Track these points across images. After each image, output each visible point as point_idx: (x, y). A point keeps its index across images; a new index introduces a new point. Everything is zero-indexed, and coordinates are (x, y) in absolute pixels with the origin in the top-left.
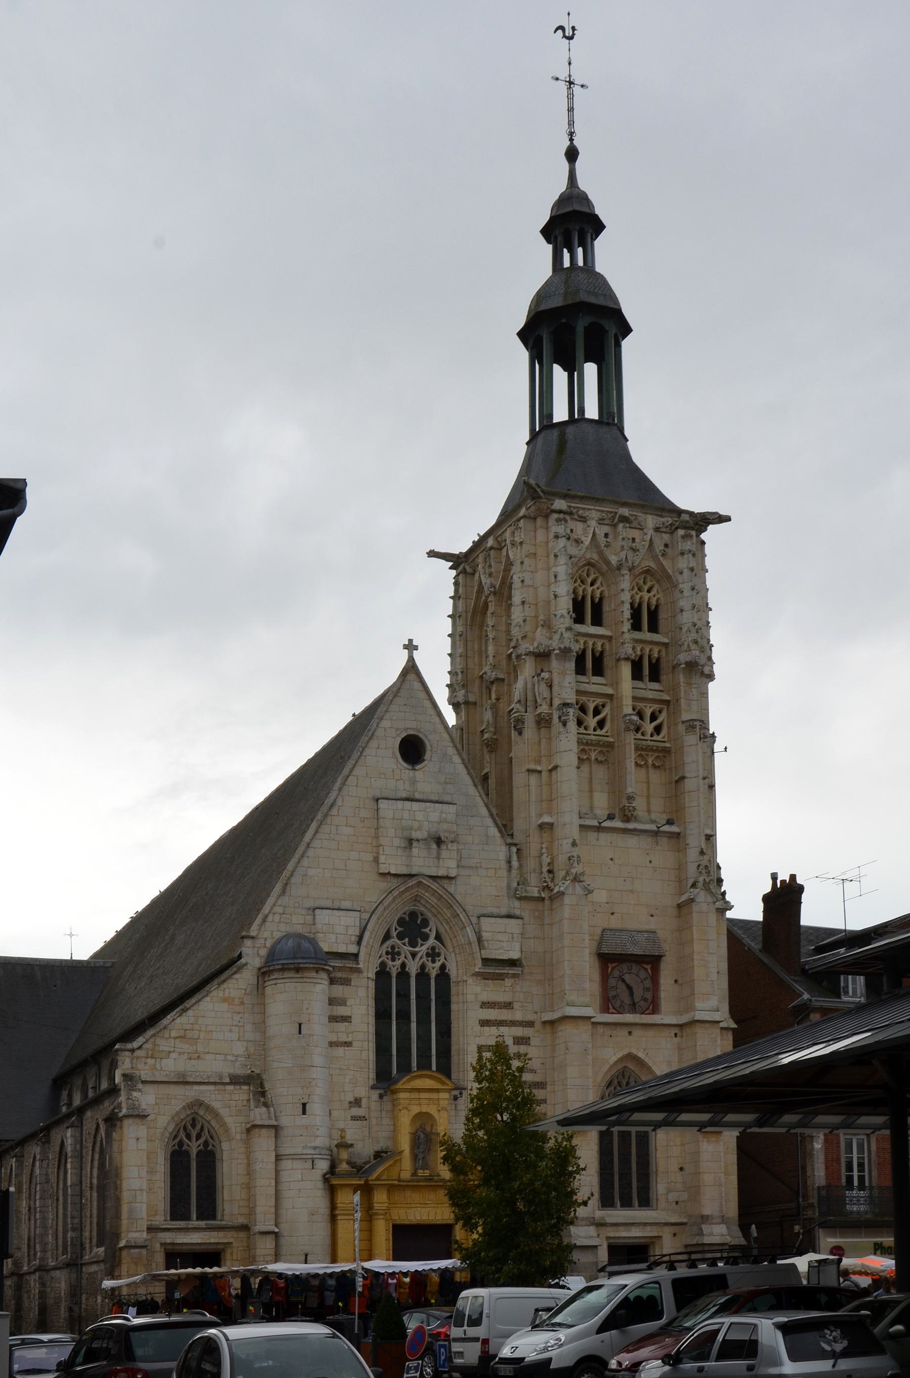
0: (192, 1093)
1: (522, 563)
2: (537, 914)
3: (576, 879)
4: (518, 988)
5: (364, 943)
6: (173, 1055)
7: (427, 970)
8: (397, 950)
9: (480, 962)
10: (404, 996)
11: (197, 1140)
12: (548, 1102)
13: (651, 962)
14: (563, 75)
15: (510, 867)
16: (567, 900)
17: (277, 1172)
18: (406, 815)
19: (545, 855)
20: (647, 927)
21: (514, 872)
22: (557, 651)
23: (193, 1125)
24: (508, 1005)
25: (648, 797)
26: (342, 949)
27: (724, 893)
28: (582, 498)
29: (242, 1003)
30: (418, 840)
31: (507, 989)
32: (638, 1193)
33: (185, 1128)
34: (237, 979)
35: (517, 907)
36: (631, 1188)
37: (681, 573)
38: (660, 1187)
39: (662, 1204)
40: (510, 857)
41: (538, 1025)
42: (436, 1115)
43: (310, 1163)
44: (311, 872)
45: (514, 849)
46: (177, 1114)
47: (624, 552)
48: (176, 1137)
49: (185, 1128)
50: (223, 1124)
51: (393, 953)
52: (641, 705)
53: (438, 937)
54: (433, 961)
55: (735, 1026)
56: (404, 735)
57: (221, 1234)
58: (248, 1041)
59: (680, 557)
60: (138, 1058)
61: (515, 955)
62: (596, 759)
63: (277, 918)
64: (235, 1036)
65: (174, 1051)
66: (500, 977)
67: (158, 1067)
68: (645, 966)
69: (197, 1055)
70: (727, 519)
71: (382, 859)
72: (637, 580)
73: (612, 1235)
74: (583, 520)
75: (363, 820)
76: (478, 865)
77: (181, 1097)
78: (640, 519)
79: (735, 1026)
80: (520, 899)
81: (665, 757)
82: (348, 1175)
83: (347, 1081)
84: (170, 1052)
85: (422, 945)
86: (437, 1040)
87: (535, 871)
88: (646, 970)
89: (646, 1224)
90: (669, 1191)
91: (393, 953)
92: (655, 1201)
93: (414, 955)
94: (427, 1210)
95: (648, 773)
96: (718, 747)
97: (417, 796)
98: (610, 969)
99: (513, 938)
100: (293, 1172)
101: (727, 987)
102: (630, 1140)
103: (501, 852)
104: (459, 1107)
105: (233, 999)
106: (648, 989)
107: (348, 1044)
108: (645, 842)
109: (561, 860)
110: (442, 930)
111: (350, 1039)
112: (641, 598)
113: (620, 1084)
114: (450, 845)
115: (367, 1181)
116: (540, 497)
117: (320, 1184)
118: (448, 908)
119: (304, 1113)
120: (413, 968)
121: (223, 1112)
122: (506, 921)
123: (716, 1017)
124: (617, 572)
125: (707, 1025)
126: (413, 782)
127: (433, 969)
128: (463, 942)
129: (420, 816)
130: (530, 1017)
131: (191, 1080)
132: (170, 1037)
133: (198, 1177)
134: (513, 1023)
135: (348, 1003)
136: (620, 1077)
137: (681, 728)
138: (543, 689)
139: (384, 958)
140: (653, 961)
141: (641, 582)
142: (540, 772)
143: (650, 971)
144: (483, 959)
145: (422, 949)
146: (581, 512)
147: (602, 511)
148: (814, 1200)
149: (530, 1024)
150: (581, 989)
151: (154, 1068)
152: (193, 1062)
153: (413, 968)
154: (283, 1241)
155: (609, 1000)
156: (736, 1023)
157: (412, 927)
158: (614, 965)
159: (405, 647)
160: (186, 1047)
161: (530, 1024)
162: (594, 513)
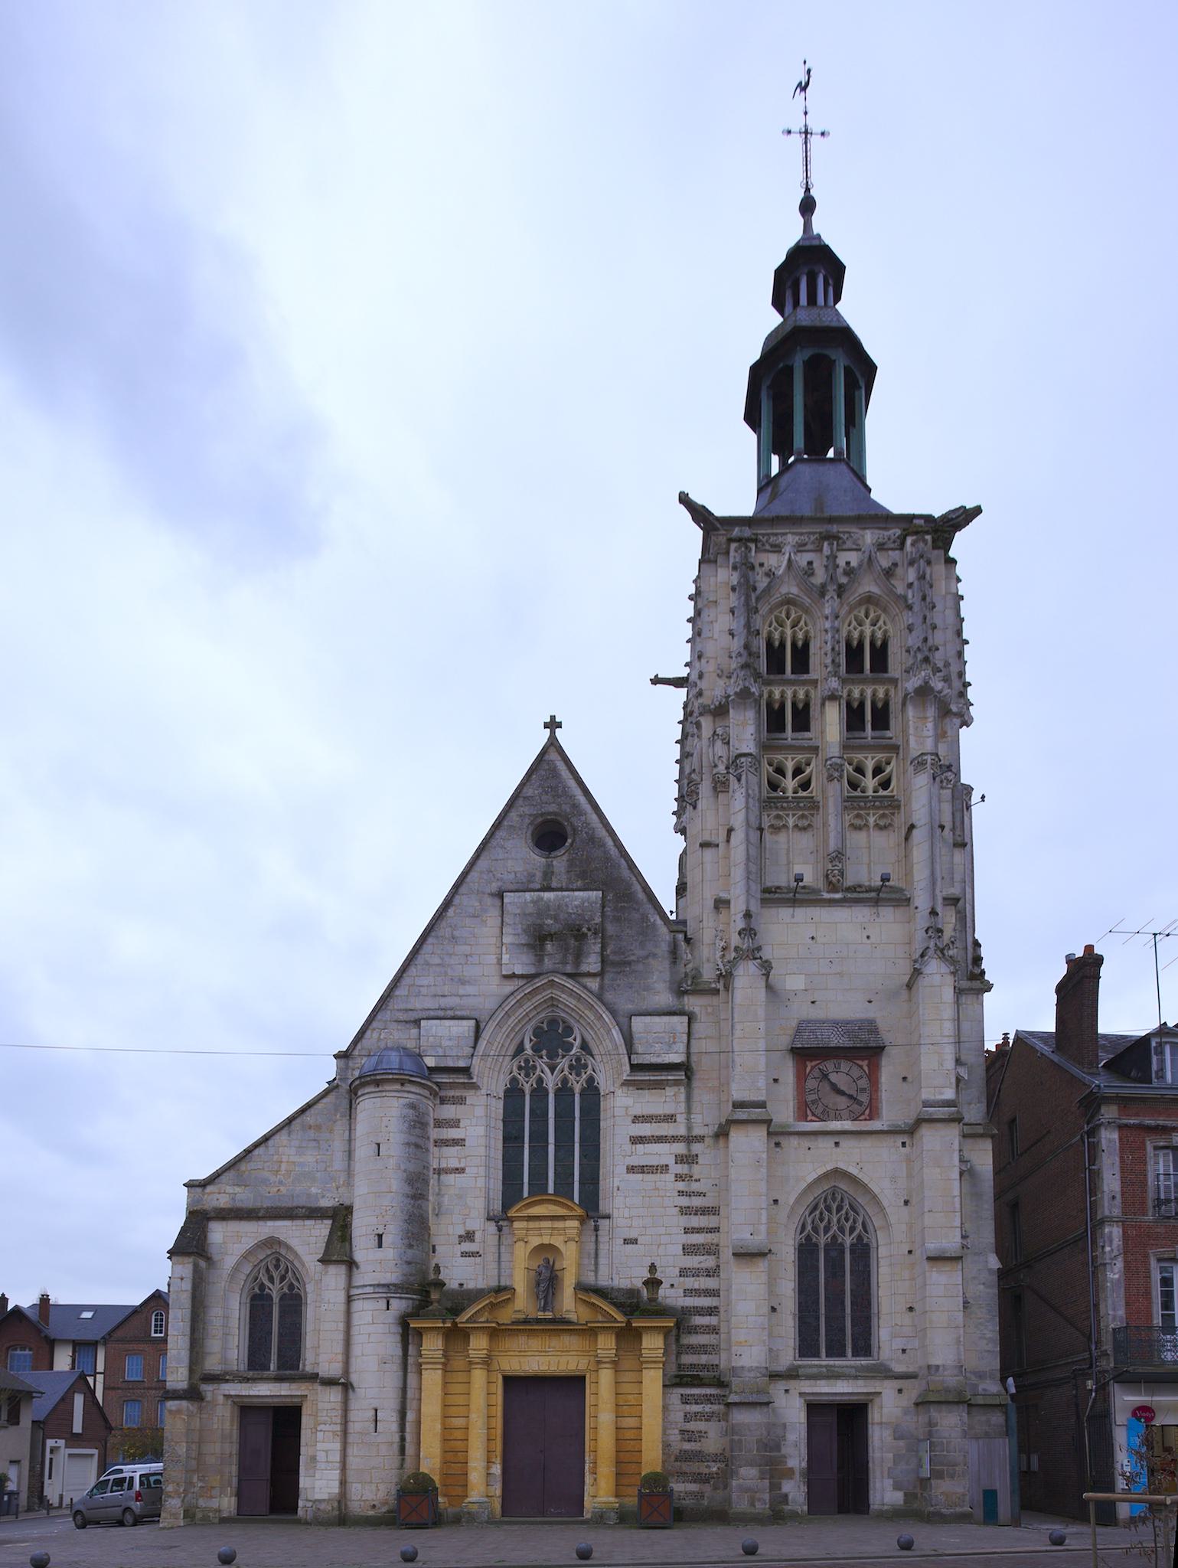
2: (710, 1010)
9: (628, 1068)
10: (539, 1116)
14: (797, 125)
17: (348, 1313)
23: (277, 1267)
33: (268, 1270)
42: (562, 1247)
49: (268, 1270)
51: (528, 1069)
52: (858, 756)
54: (578, 1075)
68: (860, 1062)
70: (978, 510)
74: (777, 549)
91: (528, 1069)
96: (975, 797)
107: (460, 1171)
110: (588, 1038)
111: (462, 1165)
113: (829, 1209)
116: (717, 529)
120: (551, 1082)
121: (299, 1249)
125: (939, 1125)
141: (862, 614)
146: (772, 539)
147: (802, 534)
148: (1108, 1346)
153: (551, 1082)
155: (807, 1105)
159: (546, 726)
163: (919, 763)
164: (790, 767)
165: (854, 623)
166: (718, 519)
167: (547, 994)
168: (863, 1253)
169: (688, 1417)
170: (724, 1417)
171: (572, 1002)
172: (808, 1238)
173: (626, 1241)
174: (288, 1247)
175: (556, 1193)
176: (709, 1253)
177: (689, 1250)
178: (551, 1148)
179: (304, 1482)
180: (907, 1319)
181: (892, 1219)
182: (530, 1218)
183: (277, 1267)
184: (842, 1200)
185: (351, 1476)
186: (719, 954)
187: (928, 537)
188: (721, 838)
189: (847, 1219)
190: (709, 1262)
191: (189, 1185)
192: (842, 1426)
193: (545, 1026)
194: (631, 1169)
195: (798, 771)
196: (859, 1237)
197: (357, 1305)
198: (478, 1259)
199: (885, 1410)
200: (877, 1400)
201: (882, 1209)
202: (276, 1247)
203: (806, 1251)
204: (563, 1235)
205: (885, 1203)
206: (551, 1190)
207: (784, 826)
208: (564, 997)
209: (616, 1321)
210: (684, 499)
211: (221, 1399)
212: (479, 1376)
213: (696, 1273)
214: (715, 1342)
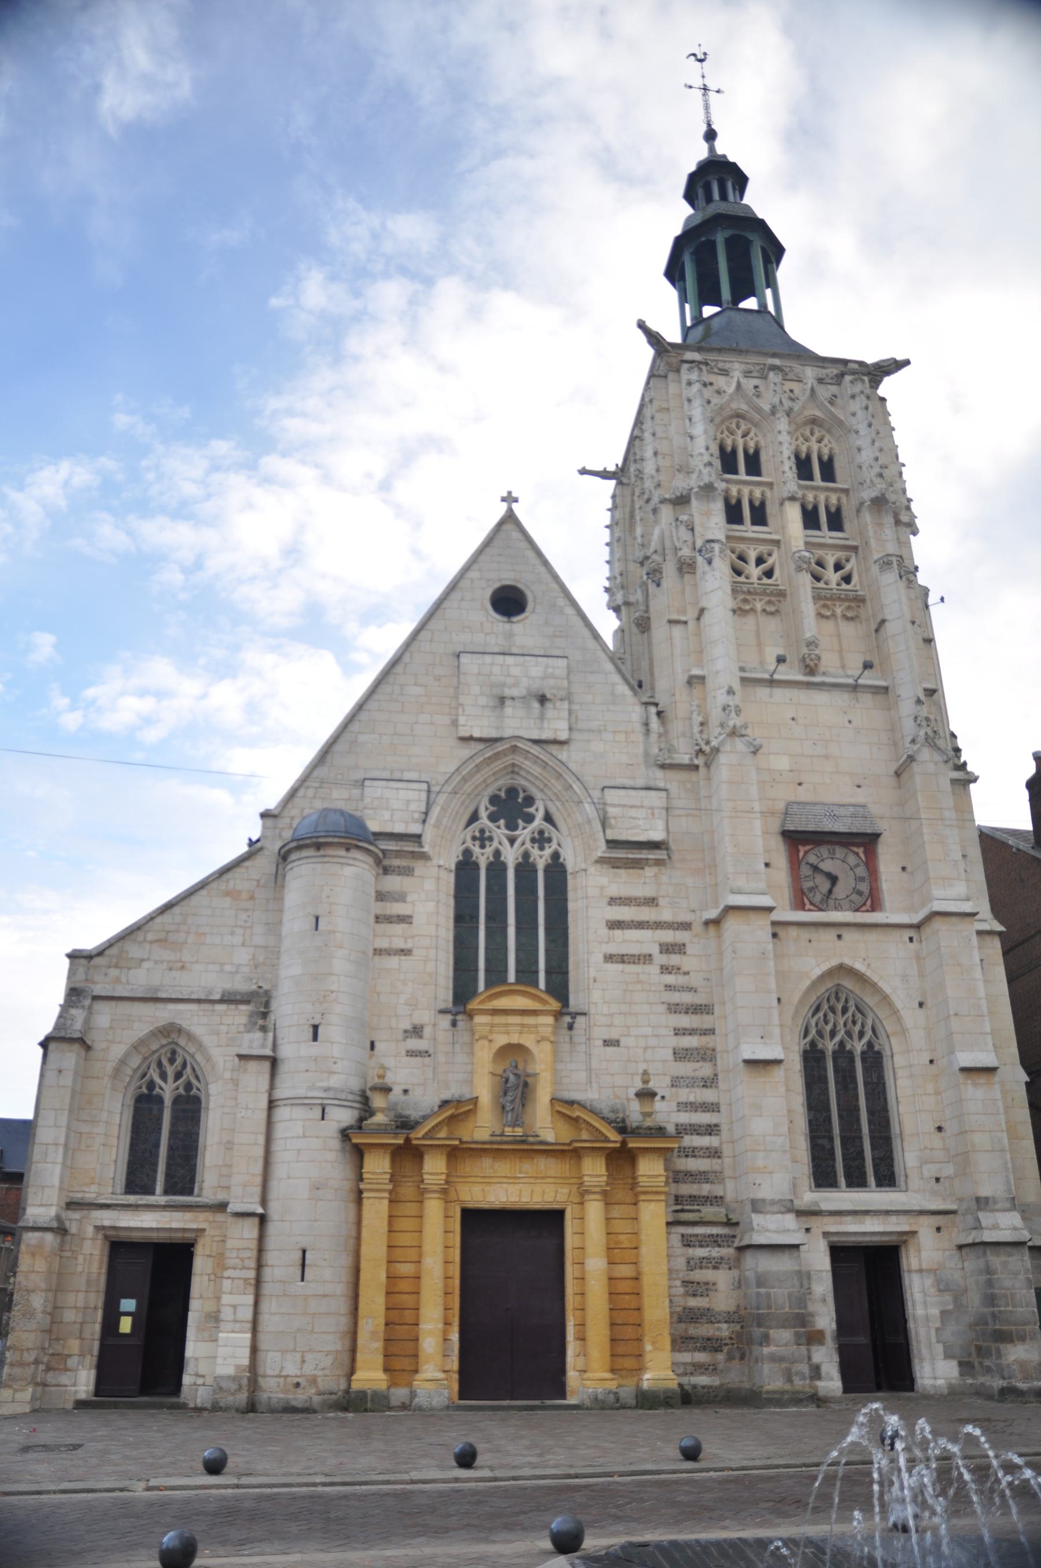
0: (165, 1014)
1: (652, 418)
2: (689, 786)
3: (734, 733)
4: (664, 879)
5: (432, 819)
6: (146, 965)
7: (531, 860)
8: (487, 834)
11: (176, 1080)
12: (717, 1032)
13: (866, 842)
15: (648, 731)
16: (723, 759)
18: (496, 670)
19: (695, 713)
20: (853, 801)
21: (654, 737)
22: (696, 490)
23: (172, 1061)
24: (651, 902)
25: (841, 652)
26: (399, 828)
27: (965, 764)
28: (720, 350)
29: (252, 898)
30: (513, 698)
31: (648, 880)
32: (875, 1166)
33: (160, 1064)
34: (247, 868)
35: (659, 777)
36: (863, 1159)
37: (854, 414)
38: (909, 1157)
39: (914, 1182)
40: (647, 718)
41: (697, 927)
43: (318, 1112)
44: (362, 738)
45: (653, 710)
46: (142, 1042)
47: (778, 396)
48: (144, 1075)
49: (160, 1064)
50: (209, 1059)
52: (820, 552)
53: (548, 818)
54: (542, 848)
55: (1002, 928)
56: (497, 585)
57: (189, 1216)
58: (256, 947)
59: (851, 401)
60: (96, 967)
61: (657, 836)
62: (764, 610)
63: (310, 793)
64: (237, 940)
65: (148, 959)
66: (638, 864)
67: (124, 979)
68: (855, 849)
69: (180, 965)
70: (907, 363)
71: (462, 720)
72: (801, 430)
73: (833, 1229)
74: (725, 372)
75: (438, 678)
76: (602, 728)
77: (148, 1019)
78: (797, 370)
79: (1002, 928)
80: (663, 767)
81: (859, 607)
82: (381, 1130)
83: (402, 1001)
84: (142, 960)
85: (524, 828)
86: (547, 950)
87: (684, 735)
88: (857, 854)
89: (887, 1213)
90: (923, 1162)
92: (902, 1178)
93: (512, 841)
94: (518, 1187)
95: (837, 625)
96: (932, 599)
97: (514, 650)
98: (801, 854)
99: (653, 814)
100: (292, 1123)
101: (984, 879)
102: (856, 1088)
103: (636, 713)
104: (576, 1039)
105: (240, 892)
106: (862, 879)
107: (405, 952)
108: (841, 699)
109: (716, 715)
110: (553, 810)
111: (409, 946)
112: (809, 449)
113: (832, 1009)
114: (558, 704)
115: (408, 1140)
117: (335, 1143)
118: (557, 779)
119: (315, 1038)
120: (511, 857)
121: (208, 1040)
122: (643, 793)
123: (967, 907)
124: (772, 417)
125: (954, 919)
126: (510, 635)
127: (541, 859)
128: (580, 820)
129: (516, 671)
130: (684, 917)
131: (164, 995)
132: (145, 941)
133: (172, 1133)
134: (658, 925)
135: (409, 899)
136: (833, 1000)
137: (875, 569)
138: (684, 534)
139: (469, 843)
140: (866, 842)
142: (686, 623)
143: (862, 856)
144: (608, 842)
145: (525, 833)
146: (720, 365)
147: (748, 363)
149: (686, 926)
150: (757, 874)
151: (118, 980)
152: (176, 974)
153: (511, 857)
154: (272, 1228)
155: (803, 893)
156: (1002, 923)
157: (511, 806)
158: (808, 847)
159: (503, 500)
160: (167, 955)
161: (686, 926)
162: (737, 367)
163: (885, 563)
164: (752, 556)
165: (801, 439)
166: (670, 344)
167: (509, 760)
168: (874, 1059)
169: (692, 1264)
170: (735, 1264)
171: (536, 770)
172: (813, 1043)
173: (607, 1043)
174: (190, 1037)
175: (518, 981)
176: (704, 1060)
177: (681, 1055)
178: (511, 931)
179: (193, 1348)
180: (937, 1140)
181: (909, 1023)
182: (495, 1012)
183: (172, 1061)
184: (847, 1001)
185: (264, 1344)
186: (696, 729)
187: (866, 379)
188: (690, 616)
189: (854, 1023)
190: (705, 1070)
191: (74, 956)
192: (870, 1272)
193: (503, 794)
194: (609, 958)
195: (760, 561)
196: (870, 1044)
197: (282, 1113)
198: (427, 1059)
199: (924, 1254)
200: (912, 1241)
201: (895, 1012)
202: (174, 1036)
203: (812, 1058)
204: (536, 1034)
205: (899, 1005)
206: (512, 977)
207: (753, 610)
208: (527, 764)
209: (607, 1140)
210: (642, 325)
211: (90, 1231)
212: (433, 1207)
213: (691, 1083)
214: (717, 1168)
